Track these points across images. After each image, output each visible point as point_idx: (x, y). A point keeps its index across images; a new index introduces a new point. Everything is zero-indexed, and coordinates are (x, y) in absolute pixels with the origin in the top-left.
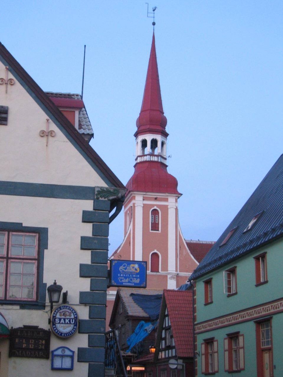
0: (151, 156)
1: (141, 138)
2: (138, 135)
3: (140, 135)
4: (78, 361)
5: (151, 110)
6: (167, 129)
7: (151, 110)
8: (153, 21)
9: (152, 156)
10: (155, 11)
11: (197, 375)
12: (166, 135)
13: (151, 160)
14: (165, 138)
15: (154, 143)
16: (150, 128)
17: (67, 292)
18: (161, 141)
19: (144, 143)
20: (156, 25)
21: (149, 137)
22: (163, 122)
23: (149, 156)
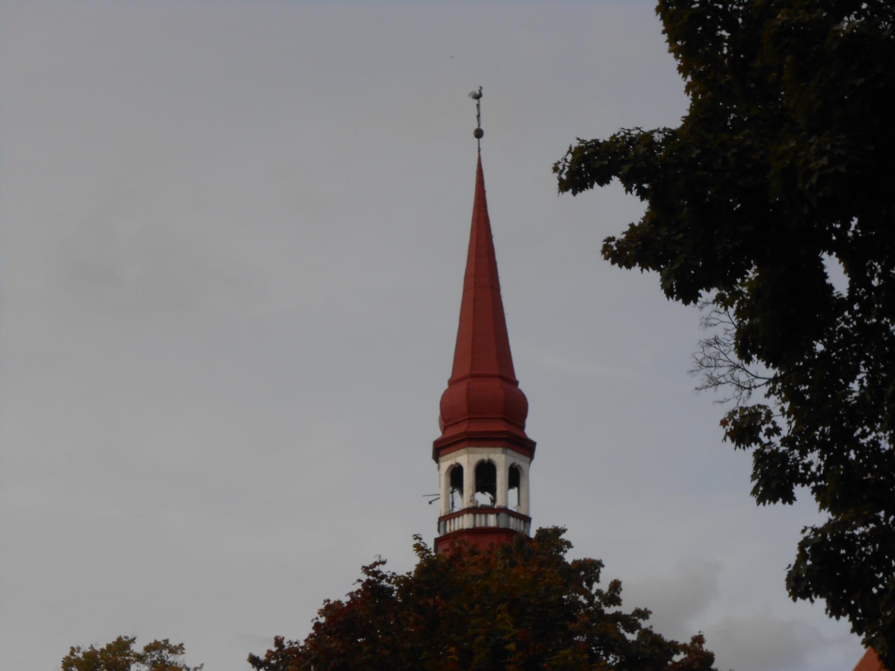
0: (474, 514)
1: (447, 463)
2: (441, 452)
3: (444, 455)
4: (620, 604)
5: (473, 376)
6: (531, 430)
7: (473, 376)
8: (481, 140)
9: (480, 514)
10: (481, 99)
11: (660, 635)
12: (527, 448)
13: (478, 525)
14: (528, 459)
15: (485, 477)
16: (470, 430)
17: (758, 504)
18: (508, 466)
19: (456, 477)
20: (485, 135)
21: (467, 459)
22: (516, 408)
23: (471, 516)
